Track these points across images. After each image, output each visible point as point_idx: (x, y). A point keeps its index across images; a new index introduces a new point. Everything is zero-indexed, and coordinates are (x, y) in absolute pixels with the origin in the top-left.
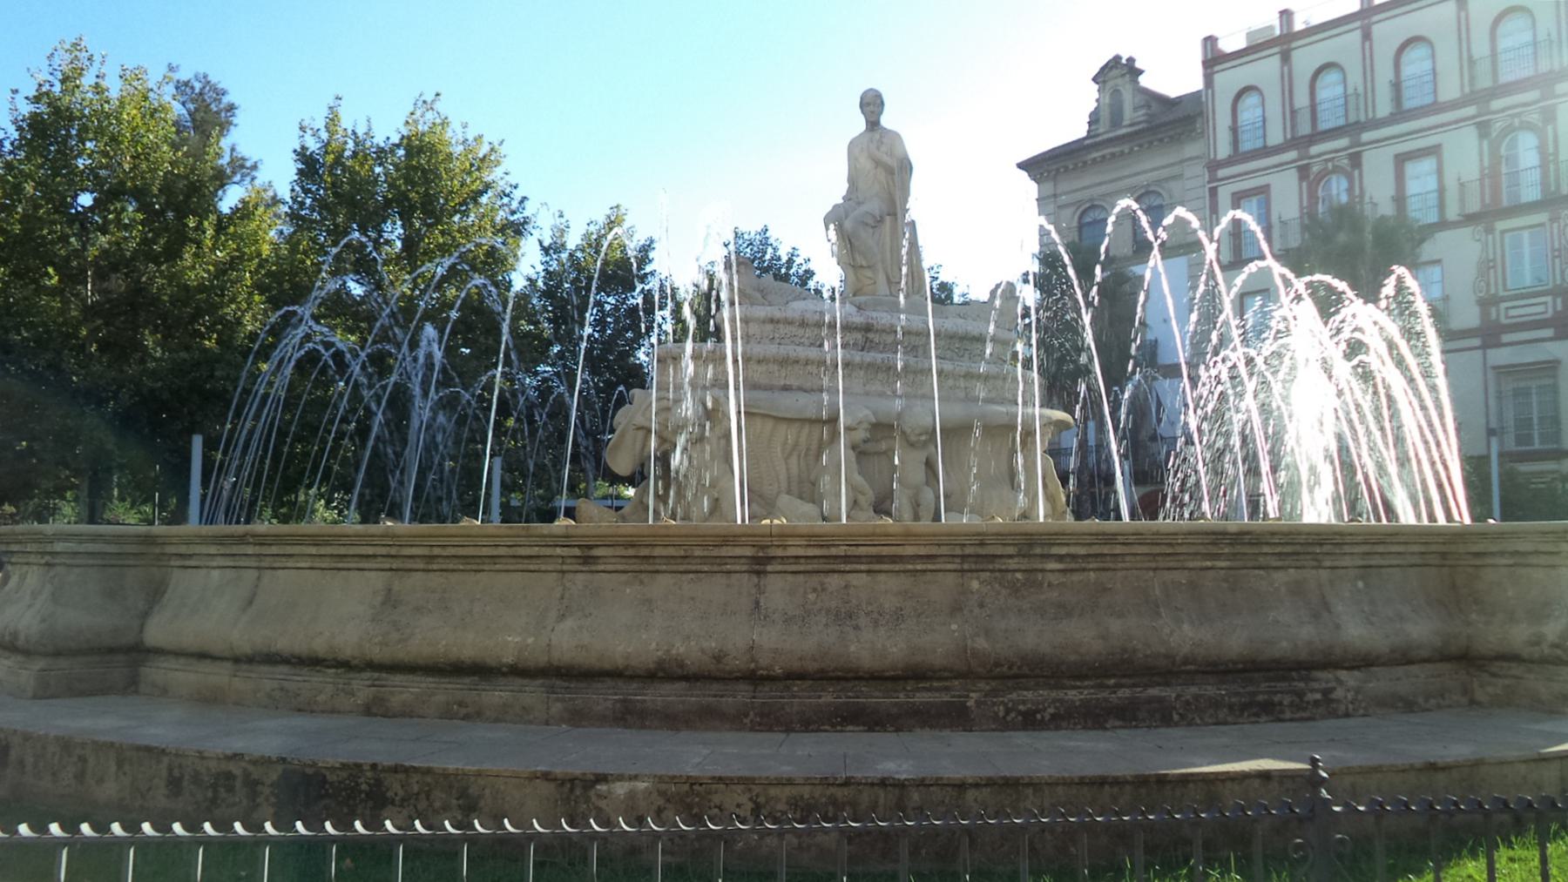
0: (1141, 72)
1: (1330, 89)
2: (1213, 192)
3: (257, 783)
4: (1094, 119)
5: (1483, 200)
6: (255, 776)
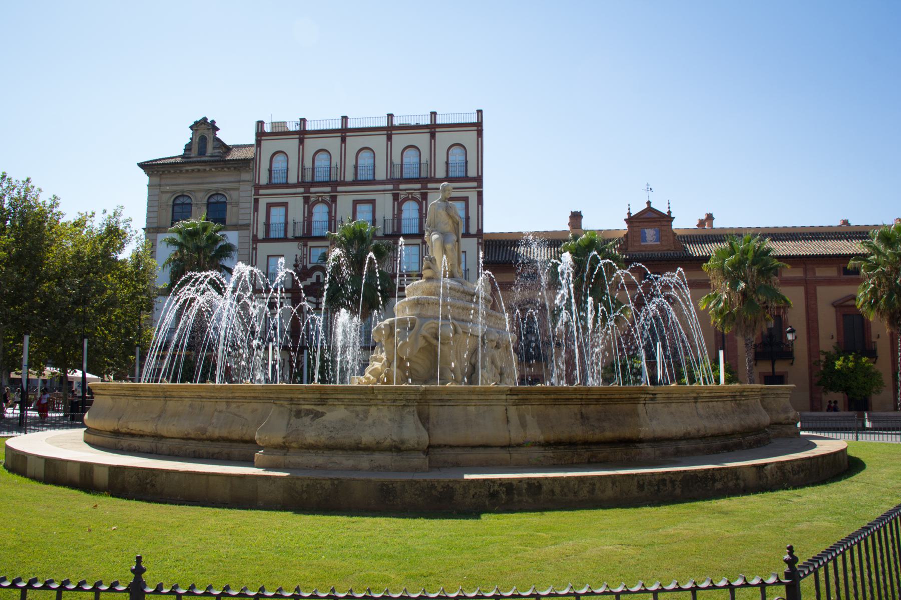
0: (218, 129)
1: (322, 161)
2: (256, 201)
3: (675, 481)
4: (188, 148)
5: (393, 229)
6: (674, 479)
